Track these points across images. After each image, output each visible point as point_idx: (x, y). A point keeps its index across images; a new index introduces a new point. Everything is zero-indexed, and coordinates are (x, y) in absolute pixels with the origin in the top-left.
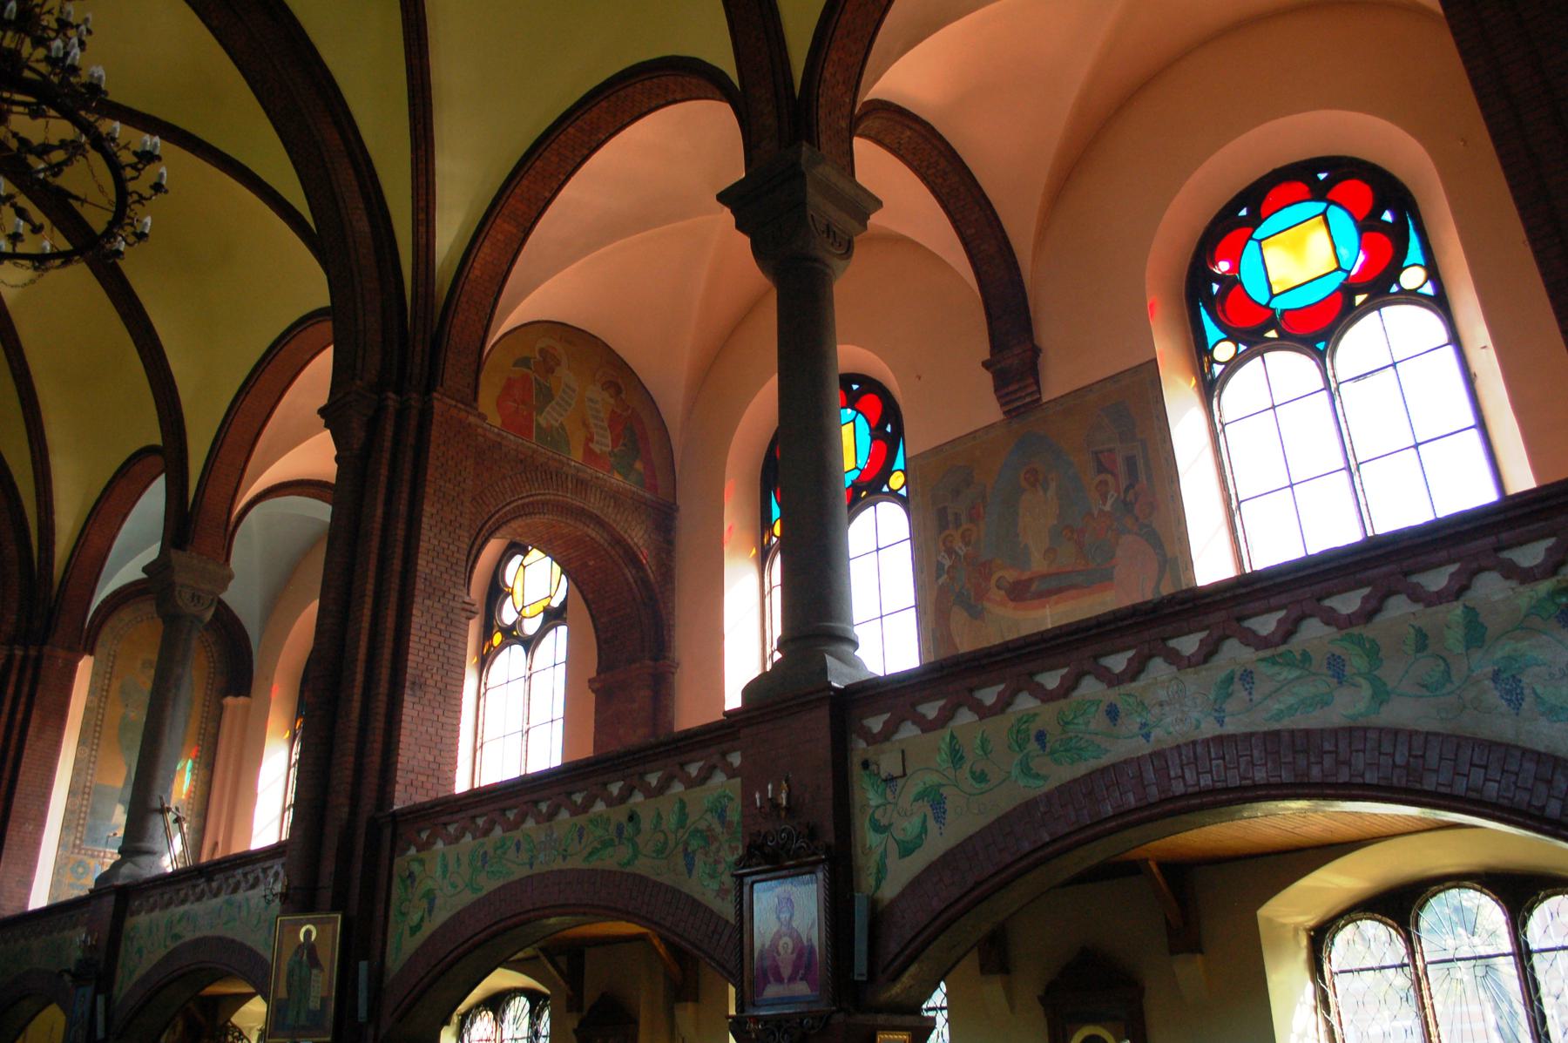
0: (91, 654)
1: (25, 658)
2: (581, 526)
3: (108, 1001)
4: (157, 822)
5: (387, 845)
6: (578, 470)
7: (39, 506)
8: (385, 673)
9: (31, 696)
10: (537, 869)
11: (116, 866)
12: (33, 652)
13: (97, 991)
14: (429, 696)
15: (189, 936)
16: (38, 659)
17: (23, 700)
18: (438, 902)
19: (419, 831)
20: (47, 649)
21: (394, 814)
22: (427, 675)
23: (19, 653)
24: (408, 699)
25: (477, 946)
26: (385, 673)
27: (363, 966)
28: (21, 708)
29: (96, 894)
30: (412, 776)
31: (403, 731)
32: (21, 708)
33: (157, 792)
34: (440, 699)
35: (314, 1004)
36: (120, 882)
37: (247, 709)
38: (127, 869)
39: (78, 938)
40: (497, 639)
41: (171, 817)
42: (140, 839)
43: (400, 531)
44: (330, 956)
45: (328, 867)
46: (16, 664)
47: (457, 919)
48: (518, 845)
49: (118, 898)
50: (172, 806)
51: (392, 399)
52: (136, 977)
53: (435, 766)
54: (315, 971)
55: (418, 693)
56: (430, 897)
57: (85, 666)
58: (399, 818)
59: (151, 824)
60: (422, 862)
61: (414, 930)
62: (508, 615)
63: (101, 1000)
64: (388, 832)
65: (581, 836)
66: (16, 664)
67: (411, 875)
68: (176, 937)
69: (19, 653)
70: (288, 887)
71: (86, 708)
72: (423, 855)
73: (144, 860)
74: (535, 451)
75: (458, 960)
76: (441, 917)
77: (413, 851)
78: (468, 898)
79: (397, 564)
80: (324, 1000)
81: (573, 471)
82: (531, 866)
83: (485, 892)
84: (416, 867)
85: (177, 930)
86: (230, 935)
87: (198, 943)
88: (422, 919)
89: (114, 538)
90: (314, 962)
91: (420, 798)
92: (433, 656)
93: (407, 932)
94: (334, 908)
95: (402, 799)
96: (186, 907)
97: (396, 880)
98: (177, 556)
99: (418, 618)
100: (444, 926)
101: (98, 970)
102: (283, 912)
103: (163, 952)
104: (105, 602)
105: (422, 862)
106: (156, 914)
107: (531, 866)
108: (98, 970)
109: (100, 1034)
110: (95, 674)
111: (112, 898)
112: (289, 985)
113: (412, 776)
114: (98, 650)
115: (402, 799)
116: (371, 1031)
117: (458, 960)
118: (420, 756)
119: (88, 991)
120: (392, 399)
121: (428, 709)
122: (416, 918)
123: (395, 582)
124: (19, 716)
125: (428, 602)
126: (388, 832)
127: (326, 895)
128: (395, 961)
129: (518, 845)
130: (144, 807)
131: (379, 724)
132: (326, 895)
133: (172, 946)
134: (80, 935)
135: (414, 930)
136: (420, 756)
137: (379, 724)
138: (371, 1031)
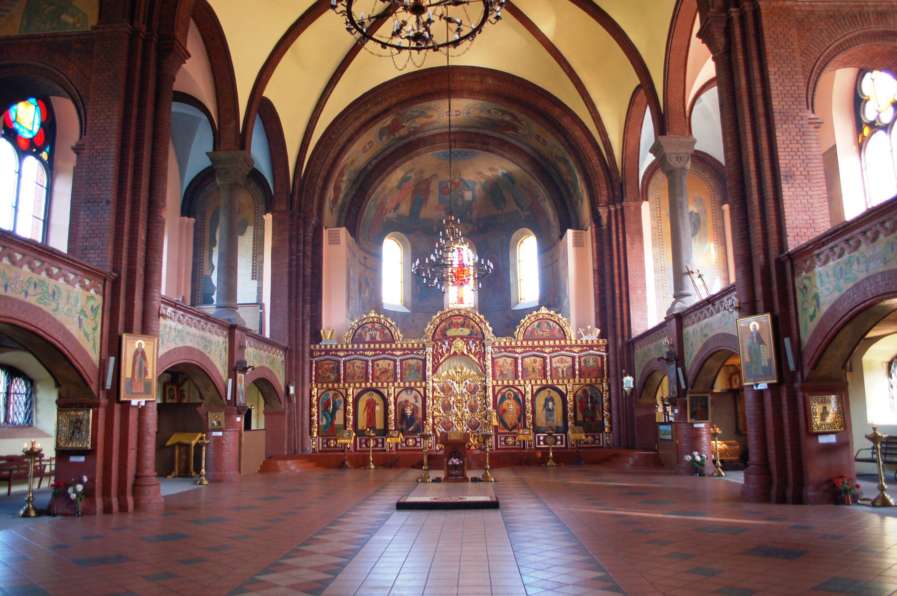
0: (647, 200)
1: (616, 210)
2: (889, 43)
3: (684, 371)
4: (687, 278)
5: (789, 272)
6: (875, 6)
7: (600, 134)
8: (768, 175)
9: (624, 229)
10: (870, 273)
11: (674, 304)
12: (619, 207)
13: (677, 367)
14: (797, 181)
15: (711, 335)
16: (622, 210)
17: (620, 231)
18: (821, 300)
19: (805, 261)
20: (624, 203)
21: (789, 255)
22: (794, 169)
23: (612, 209)
24: (785, 187)
25: (846, 323)
26: (768, 175)
27: (787, 341)
28: (621, 235)
29: (668, 319)
30: (797, 230)
31: (785, 206)
32: (621, 235)
33: (685, 264)
34: (806, 181)
35: (765, 363)
36: (676, 312)
37: (867, 204)
38: (677, 305)
39: (665, 342)
40: (866, 131)
41: (695, 276)
42: (682, 290)
43: (758, 90)
44: (768, 337)
45: (759, 290)
46: (613, 215)
47: (833, 308)
48: (858, 259)
49: (678, 319)
50: (695, 271)
51: (734, 12)
52: (693, 358)
53: (811, 221)
54: (762, 346)
55: (791, 181)
56: (816, 297)
57: (645, 207)
58: (792, 257)
59: (685, 281)
60: (809, 279)
61: (812, 317)
62: (869, 114)
63: (680, 369)
64: (788, 264)
65: (893, 249)
66: (613, 215)
67: (805, 287)
68: (705, 335)
69: (612, 209)
70: (739, 303)
71: (652, 228)
72: (809, 274)
73: (686, 299)
74: (839, 7)
75: (839, 331)
76: (824, 308)
77: (804, 274)
78: (837, 295)
79: (761, 109)
80: (769, 361)
81: (872, 9)
82: (867, 270)
83: (844, 290)
84: (806, 282)
85: (705, 332)
86: (727, 332)
87: (716, 337)
88: (815, 311)
89: (640, 138)
90: (760, 341)
91: (803, 242)
92: (795, 157)
93: (808, 319)
94: (766, 311)
95: (792, 245)
96: (707, 320)
97: (798, 292)
98: (663, 139)
99: (779, 134)
100: (827, 313)
101: (677, 357)
102: (741, 317)
103: (701, 344)
104: (646, 173)
105: (809, 279)
106: (695, 325)
107: (867, 270)
108: (677, 357)
109: (683, 387)
110: (652, 209)
111: (674, 321)
112: (750, 354)
113: (797, 230)
114: (650, 197)
115: (792, 245)
116: (799, 376)
117: (839, 331)
118: (799, 217)
119: (673, 366)
120: (734, 12)
121: (799, 189)
122: (811, 310)
123: (762, 120)
124: (621, 239)
125: (785, 126)
126: (788, 264)
127: (760, 305)
128: (805, 337)
129: (858, 259)
130: (680, 274)
131: (770, 204)
132: (760, 305)
133: (705, 340)
134: (665, 341)
135: (812, 317)
136: (799, 217)
137: (770, 204)
138: (799, 376)
